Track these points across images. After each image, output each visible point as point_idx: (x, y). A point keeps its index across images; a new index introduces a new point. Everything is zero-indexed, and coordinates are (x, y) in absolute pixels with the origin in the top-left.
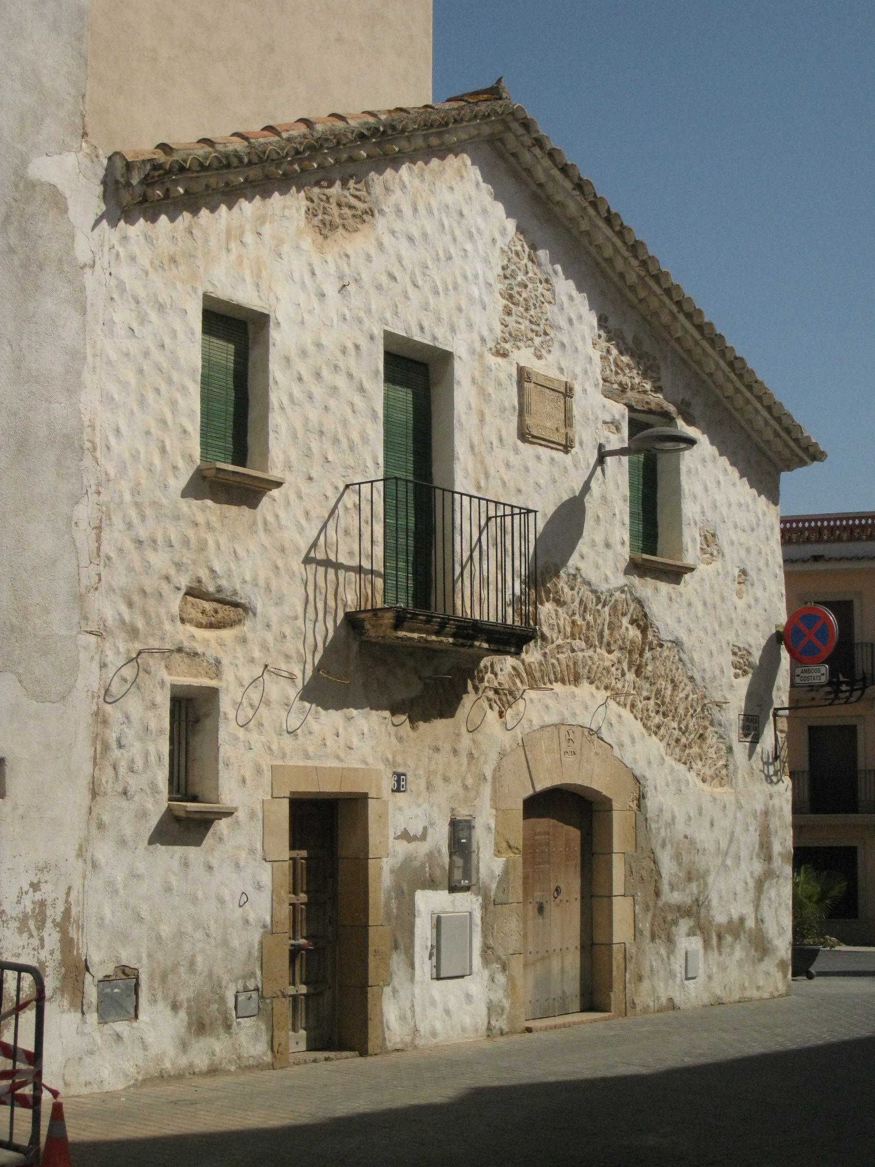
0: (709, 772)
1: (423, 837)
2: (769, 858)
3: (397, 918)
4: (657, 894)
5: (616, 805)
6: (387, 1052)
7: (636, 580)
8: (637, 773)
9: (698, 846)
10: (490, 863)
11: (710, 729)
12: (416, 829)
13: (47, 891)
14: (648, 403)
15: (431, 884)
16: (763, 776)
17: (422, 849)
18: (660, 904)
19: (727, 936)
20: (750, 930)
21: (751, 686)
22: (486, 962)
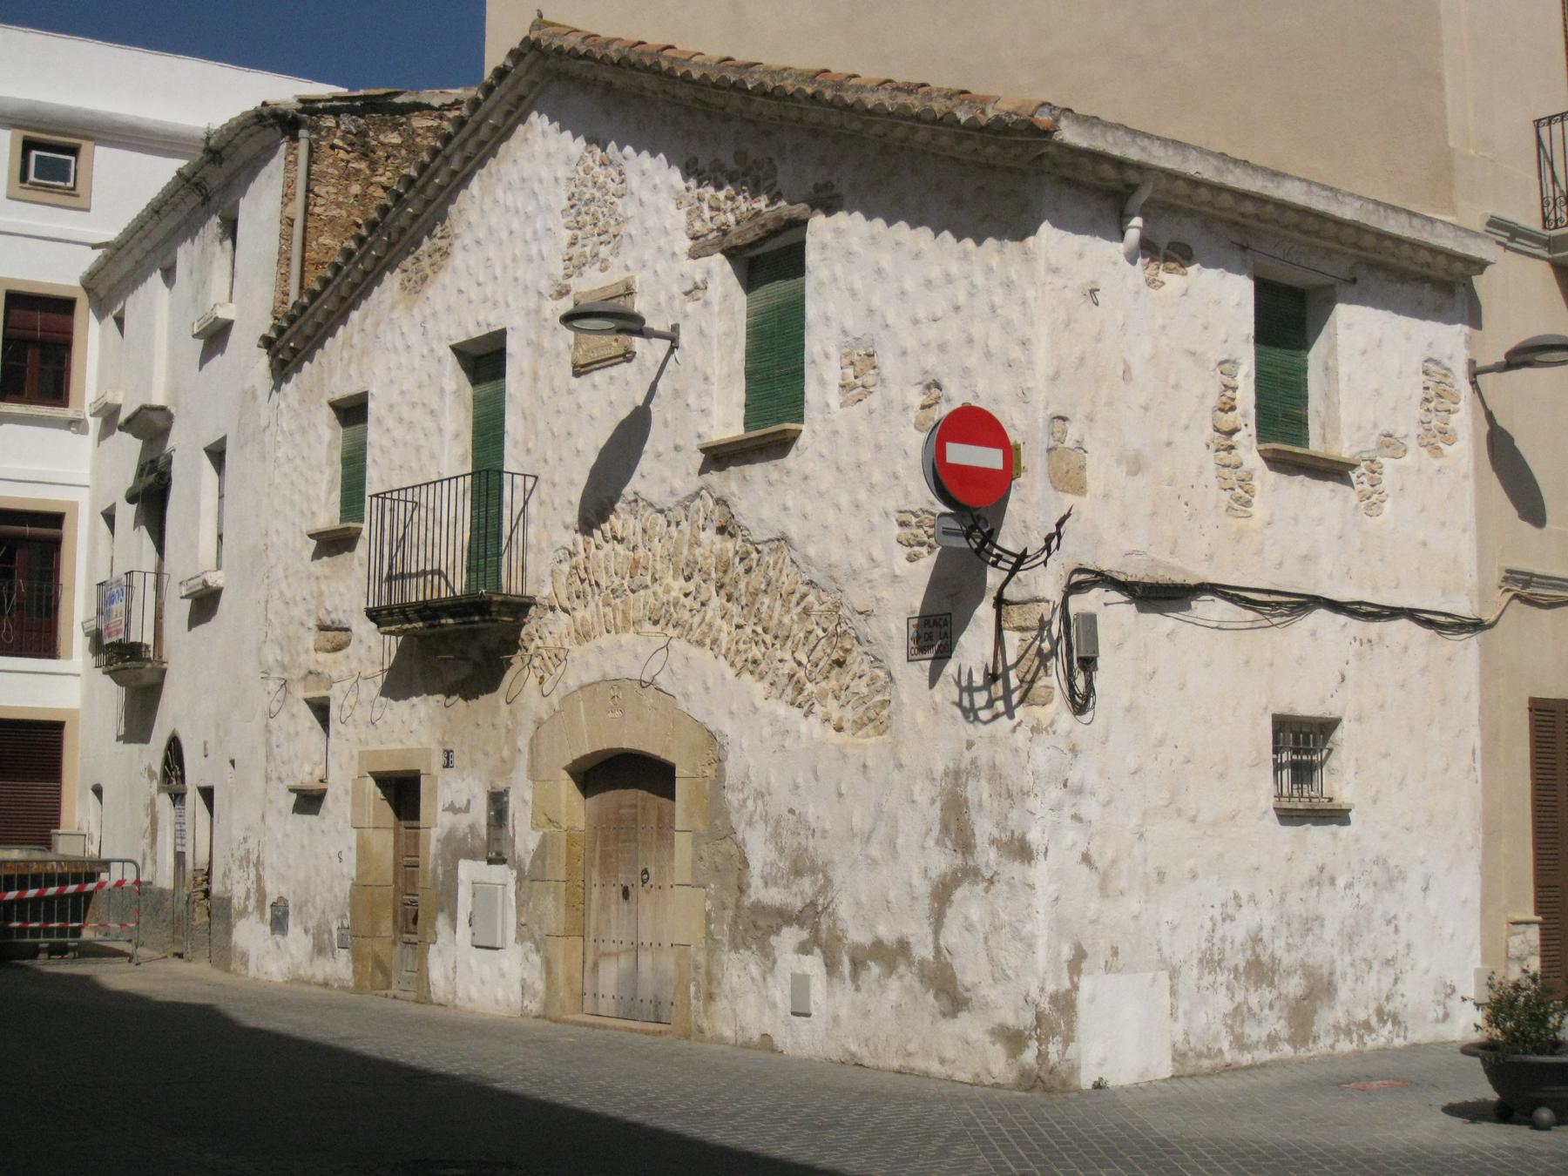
0: (849, 715)
1: (467, 809)
2: (965, 845)
3: (443, 883)
4: (742, 889)
5: (679, 772)
6: (431, 1003)
7: (714, 477)
8: (712, 728)
9: (813, 824)
10: (525, 837)
11: (858, 649)
12: (461, 802)
13: (252, 844)
14: (763, 226)
15: (472, 856)
16: (958, 712)
17: (463, 821)
18: (747, 902)
19: (871, 964)
20: (923, 962)
21: (937, 564)
22: (520, 939)
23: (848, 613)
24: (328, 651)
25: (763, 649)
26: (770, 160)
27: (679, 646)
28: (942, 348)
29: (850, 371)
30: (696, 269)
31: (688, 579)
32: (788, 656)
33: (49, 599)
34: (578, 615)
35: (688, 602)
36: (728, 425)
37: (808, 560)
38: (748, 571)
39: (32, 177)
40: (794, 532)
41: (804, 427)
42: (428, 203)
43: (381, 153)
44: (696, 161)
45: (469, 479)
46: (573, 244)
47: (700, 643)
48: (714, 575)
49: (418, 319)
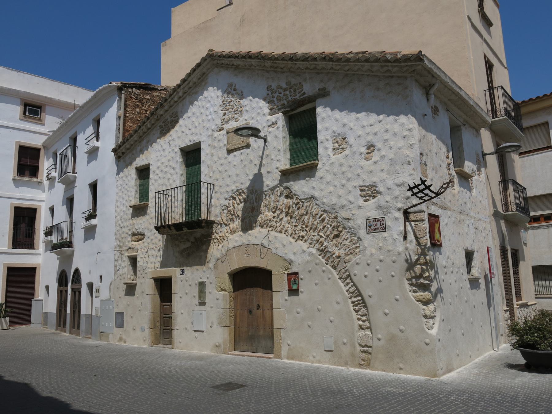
23: (341, 219)
24: (136, 241)
25: (305, 232)
26: (300, 83)
27: (273, 233)
28: (375, 134)
29: (336, 144)
30: (273, 118)
31: (274, 212)
32: (316, 234)
33: (32, 233)
34: (231, 226)
35: (275, 220)
36: (286, 165)
37: (324, 203)
38: (298, 209)
39: (27, 114)
40: (316, 194)
41: (319, 162)
42: (171, 106)
43: (144, 101)
44: (271, 86)
45: (184, 187)
46: (224, 115)
47: (281, 232)
48: (284, 210)
49: (167, 141)
